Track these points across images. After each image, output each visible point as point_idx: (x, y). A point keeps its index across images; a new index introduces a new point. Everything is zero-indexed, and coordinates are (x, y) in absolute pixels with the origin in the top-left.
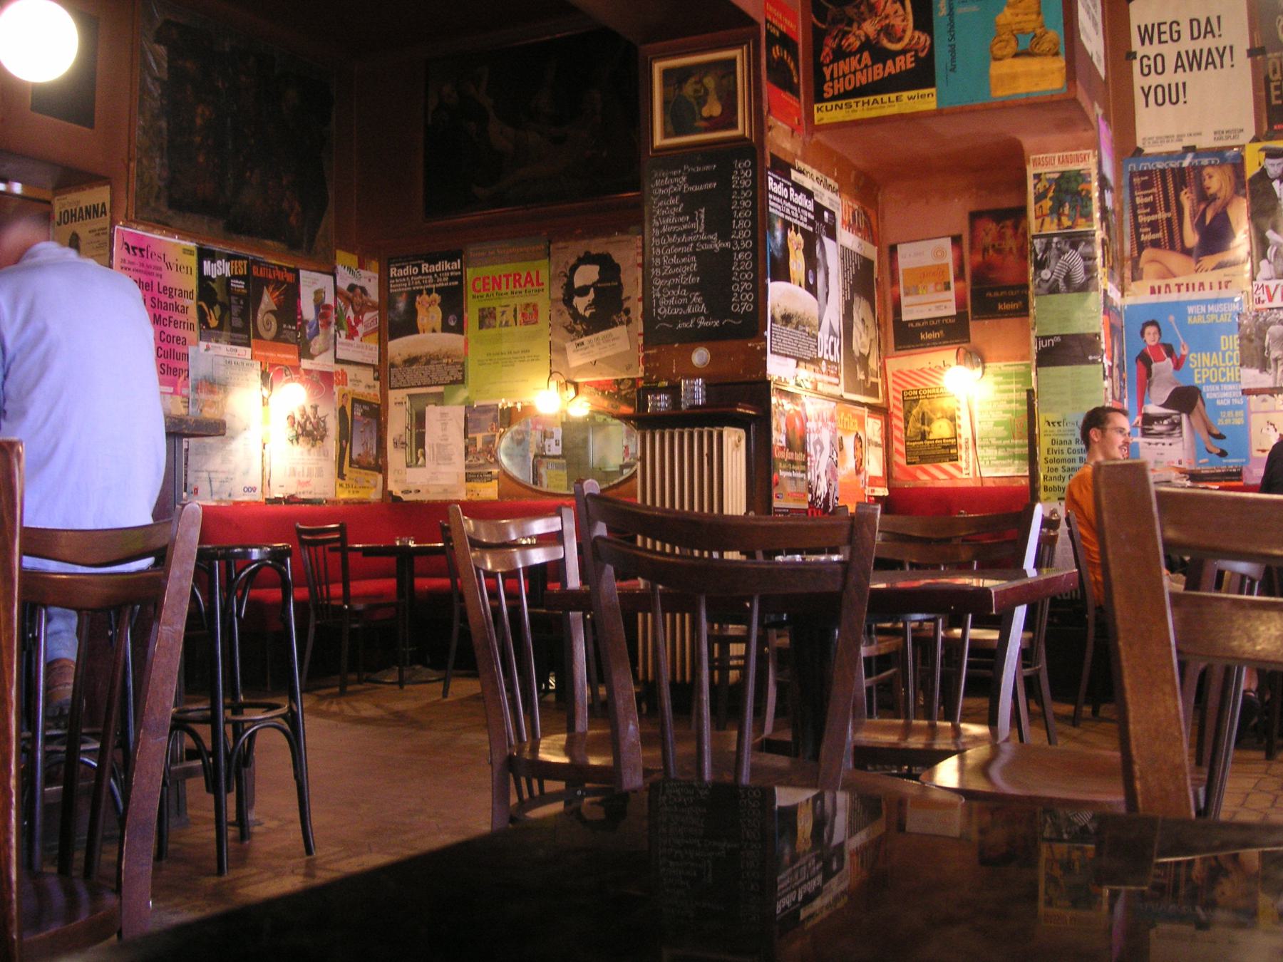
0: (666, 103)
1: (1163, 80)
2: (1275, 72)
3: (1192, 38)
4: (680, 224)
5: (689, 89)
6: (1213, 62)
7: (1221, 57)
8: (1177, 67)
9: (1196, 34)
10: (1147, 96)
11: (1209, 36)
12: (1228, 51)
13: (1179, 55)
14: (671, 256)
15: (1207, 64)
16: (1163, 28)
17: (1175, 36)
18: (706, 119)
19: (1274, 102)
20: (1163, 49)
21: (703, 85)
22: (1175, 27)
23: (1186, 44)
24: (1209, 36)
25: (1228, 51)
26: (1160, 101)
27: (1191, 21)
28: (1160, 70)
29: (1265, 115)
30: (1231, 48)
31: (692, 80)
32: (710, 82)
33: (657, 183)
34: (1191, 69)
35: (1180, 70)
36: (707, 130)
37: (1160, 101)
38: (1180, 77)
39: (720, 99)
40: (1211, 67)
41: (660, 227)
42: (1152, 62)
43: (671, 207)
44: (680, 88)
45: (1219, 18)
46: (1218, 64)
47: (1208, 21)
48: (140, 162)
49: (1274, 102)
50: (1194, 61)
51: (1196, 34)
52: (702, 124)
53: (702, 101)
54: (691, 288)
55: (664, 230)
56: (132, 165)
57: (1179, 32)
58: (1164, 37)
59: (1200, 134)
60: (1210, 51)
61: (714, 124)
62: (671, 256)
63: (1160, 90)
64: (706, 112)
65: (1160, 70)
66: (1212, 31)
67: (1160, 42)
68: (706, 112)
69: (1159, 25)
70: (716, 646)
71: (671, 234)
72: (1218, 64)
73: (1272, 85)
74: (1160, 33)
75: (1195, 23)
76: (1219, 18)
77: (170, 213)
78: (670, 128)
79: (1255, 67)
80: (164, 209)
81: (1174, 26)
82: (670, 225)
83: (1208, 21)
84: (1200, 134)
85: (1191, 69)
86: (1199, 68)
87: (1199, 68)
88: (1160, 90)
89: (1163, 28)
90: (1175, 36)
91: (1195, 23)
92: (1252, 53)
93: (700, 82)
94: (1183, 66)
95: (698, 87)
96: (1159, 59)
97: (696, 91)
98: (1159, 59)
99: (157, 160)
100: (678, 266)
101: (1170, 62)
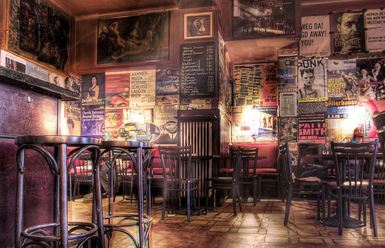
0: (188, 27)
1: (307, 39)
2: (336, 38)
3: (315, 28)
4: (192, 65)
5: (195, 23)
6: (320, 35)
7: (323, 33)
8: (311, 35)
9: (316, 27)
10: (303, 43)
11: (319, 28)
12: (324, 32)
13: (311, 32)
14: (187, 76)
15: (319, 35)
16: (307, 25)
17: (311, 27)
18: (201, 32)
19: (336, 46)
20: (307, 31)
21: (200, 22)
22: (311, 25)
23: (313, 30)
24: (319, 28)
25: (324, 32)
26: (306, 44)
27: (315, 24)
28: (306, 36)
29: (333, 50)
30: (325, 31)
31: (196, 20)
32: (202, 21)
33: (184, 51)
34: (315, 36)
35: (312, 36)
36: (200, 35)
37: (306, 44)
38: (312, 38)
39: (205, 26)
40: (320, 36)
42: (304, 34)
43: (188, 59)
44: (193, 23)
45: (322, 23)
46: (322, 35)
47: (319, 24)
48: (10, 32)
49: (336, 46)
50: (315, 34)
51: (316, 27)
52: (199, 33)
53: (199, 27)
54: (194, 85)
55: (186, 67)
56: (7, 32)
57: (311, 26)
58: (308, 28)
59: (316, 53)
60: (319, 32)
61: (202, 33)
62: (187, 76)
63: (306, 41)
64: (200, 30)
65: (306, 36)
66: (320, 27)
67: (307, 29)
68: (200, 30)
69: (306, 24)
70: (118, 77)
71: (188, 69)
72: (322, 35)
73: (335, 41)
74: (306, 26)
75: (316, 25)
76: (322, 23)
77: (20, 50)
78: (189, 34)
79: (331, 36)
80: (18, 49)
81: (310, 25)
82: (188, 66)
83: (319, 24)
84: (316, 53)
85: (315, 36)
86: (317, 36)
87: (317, 36)
88: (306, 41)
89: (307, 25)
90: (311, 27)
91: (316, 25)
92: (331, 33)
93: (199, 21)
94: (312, 35)
95: (198, 22)
96: (306, 33)
97: (197, 24)
98: (306, 33)
99: (16, 33)
100: (190, 79)
101: (309, 34)
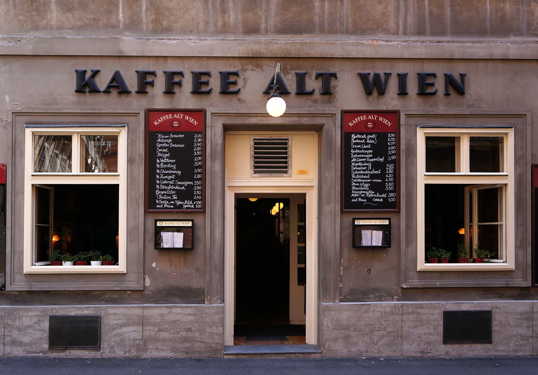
41: (159, 164)
